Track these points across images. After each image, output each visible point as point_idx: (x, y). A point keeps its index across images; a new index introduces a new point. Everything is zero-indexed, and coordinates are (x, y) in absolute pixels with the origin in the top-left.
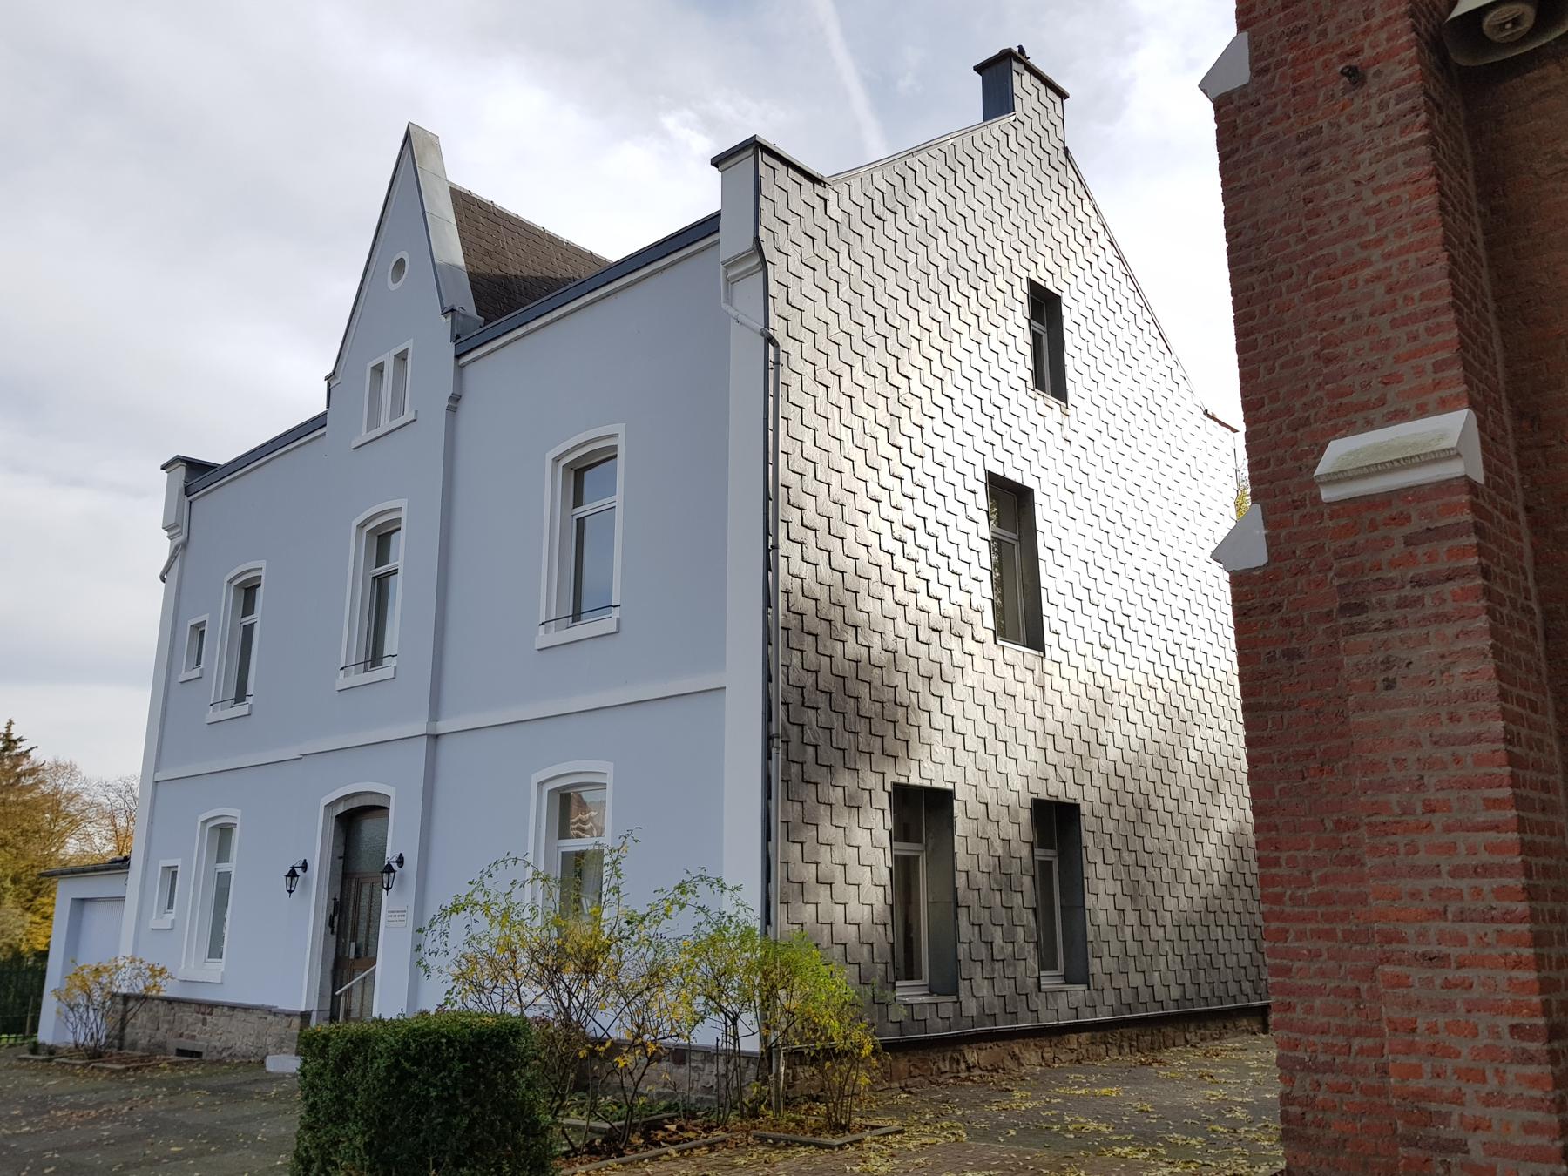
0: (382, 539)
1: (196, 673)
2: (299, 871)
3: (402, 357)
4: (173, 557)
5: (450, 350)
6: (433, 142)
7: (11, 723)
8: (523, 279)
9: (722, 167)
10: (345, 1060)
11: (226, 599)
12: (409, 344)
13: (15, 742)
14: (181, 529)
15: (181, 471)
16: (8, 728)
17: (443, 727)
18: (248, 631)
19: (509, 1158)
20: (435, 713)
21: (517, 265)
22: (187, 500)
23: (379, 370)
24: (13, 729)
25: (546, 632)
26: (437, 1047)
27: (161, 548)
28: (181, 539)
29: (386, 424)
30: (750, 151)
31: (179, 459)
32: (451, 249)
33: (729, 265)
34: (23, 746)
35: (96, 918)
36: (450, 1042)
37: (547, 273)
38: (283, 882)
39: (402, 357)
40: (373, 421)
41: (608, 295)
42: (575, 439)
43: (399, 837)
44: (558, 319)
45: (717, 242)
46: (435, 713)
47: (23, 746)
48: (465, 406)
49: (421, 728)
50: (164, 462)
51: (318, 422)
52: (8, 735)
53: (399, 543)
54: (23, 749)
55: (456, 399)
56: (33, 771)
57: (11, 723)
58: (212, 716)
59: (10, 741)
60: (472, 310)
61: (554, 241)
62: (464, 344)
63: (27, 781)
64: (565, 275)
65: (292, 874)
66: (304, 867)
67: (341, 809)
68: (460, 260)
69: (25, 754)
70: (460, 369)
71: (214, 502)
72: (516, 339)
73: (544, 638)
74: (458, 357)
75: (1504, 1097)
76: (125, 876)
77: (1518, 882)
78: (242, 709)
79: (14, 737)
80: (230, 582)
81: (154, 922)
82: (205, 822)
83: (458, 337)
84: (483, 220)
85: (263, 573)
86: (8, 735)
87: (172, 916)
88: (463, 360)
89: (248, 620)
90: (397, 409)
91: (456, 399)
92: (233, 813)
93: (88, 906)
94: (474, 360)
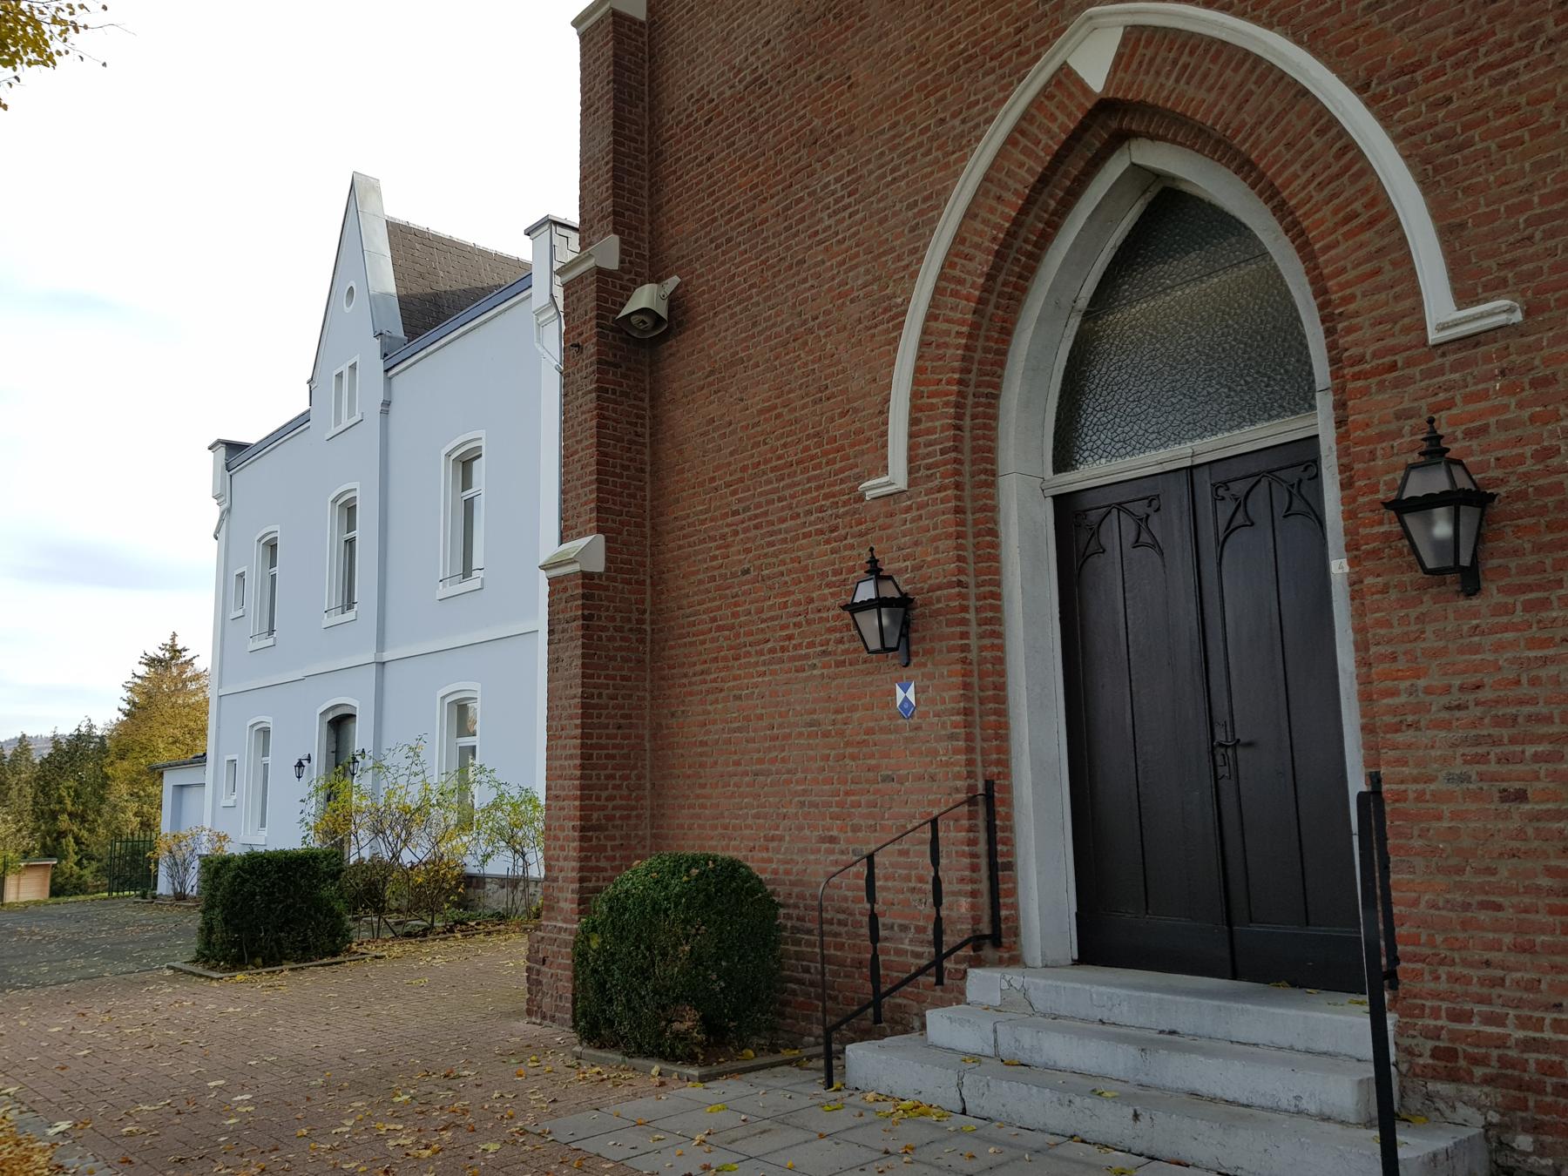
0: (349, 510)
1: (240, 613)
2: (305, 763)
3: (353, 367)
4: (221, 520)
5: (380, 365)
6: (374, 187)
7: (175, 635)
8: (453, 293)
9: (533, 235)
10: (217, 871)
11: (256, 553)
12: (357, 359)
13: (180, 652)
14: (226, 497)
15: (222, 451)
16: (173, 639)
17: (387, 656)
18: (469, 505)
19: (312, 930)
20: (381, 645)
21: (448, 281)
22: (228, 474)
23: (340, 376)
24: (177, 640)
25: (444, 586)
26: (261, 865)
27: (213, 512)
28: (226, 506)
29: (346, 423)
30: (547, 227)
31: (220, 442)
32: (386, 281)
33: (539, 313)
34: (188, 656)
35: (190, 797)
36: (269, 862)
37: (474, 284)
38: (293, 772)
39: (353, 367)
40: (338, 421)
41: (485, 322)
42: (457, 441)
43: (361, 737)
44: (445, 345)
45: (531, 295)
46: (381, 645)
47: (188, 656)
48: (393, 408)
49: (370, 657)
50: (210, 444)
51: (303, 419)
52: (173, 646)
53: (479, 468)
54: (187, 658)
55: (387, 404)
56: (197, 677)
57: (175, 635)
58: (253, 646)
59: (175, 651)
60: (402, 334)
61: (484, 253)
62: (392, 357)
63: (192, 686)
64: (491, 283)
65: (300, 765)
66: (309, 760)
67: (330, 716)
68: (392, 289)
69: (189, 662)
70: (388, 381)
71: (249, 475)
72: (421, 359)
73: (443, 591)
74: (387, 371)
75: (142, 823)
76: (202, 769)
77: (578, 762)
78: (350, 615)
79: (179, 647)
80: (259, 541)
81: (224, 802)
82: (252, 726)
83: (386, 355)
84: (418, 246)
85: (482, 443)
86: (173, 646)
87: (234, 797)
88: (391, 373)
89: (468, 494)
90: (351, 414)
91: (387, 404)
92: (269, 721)
93: (185, 789)
94: (397, 374)
